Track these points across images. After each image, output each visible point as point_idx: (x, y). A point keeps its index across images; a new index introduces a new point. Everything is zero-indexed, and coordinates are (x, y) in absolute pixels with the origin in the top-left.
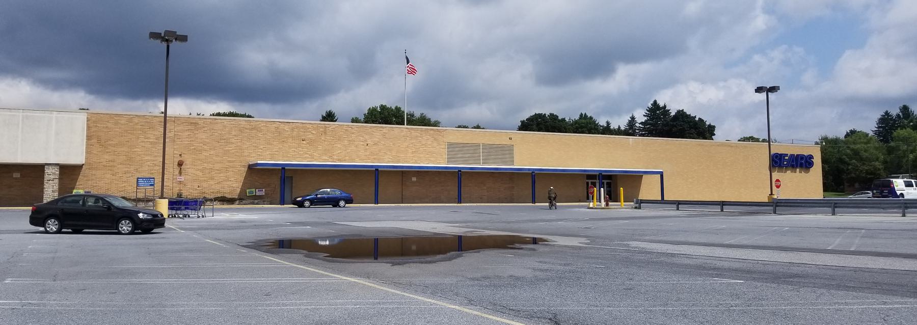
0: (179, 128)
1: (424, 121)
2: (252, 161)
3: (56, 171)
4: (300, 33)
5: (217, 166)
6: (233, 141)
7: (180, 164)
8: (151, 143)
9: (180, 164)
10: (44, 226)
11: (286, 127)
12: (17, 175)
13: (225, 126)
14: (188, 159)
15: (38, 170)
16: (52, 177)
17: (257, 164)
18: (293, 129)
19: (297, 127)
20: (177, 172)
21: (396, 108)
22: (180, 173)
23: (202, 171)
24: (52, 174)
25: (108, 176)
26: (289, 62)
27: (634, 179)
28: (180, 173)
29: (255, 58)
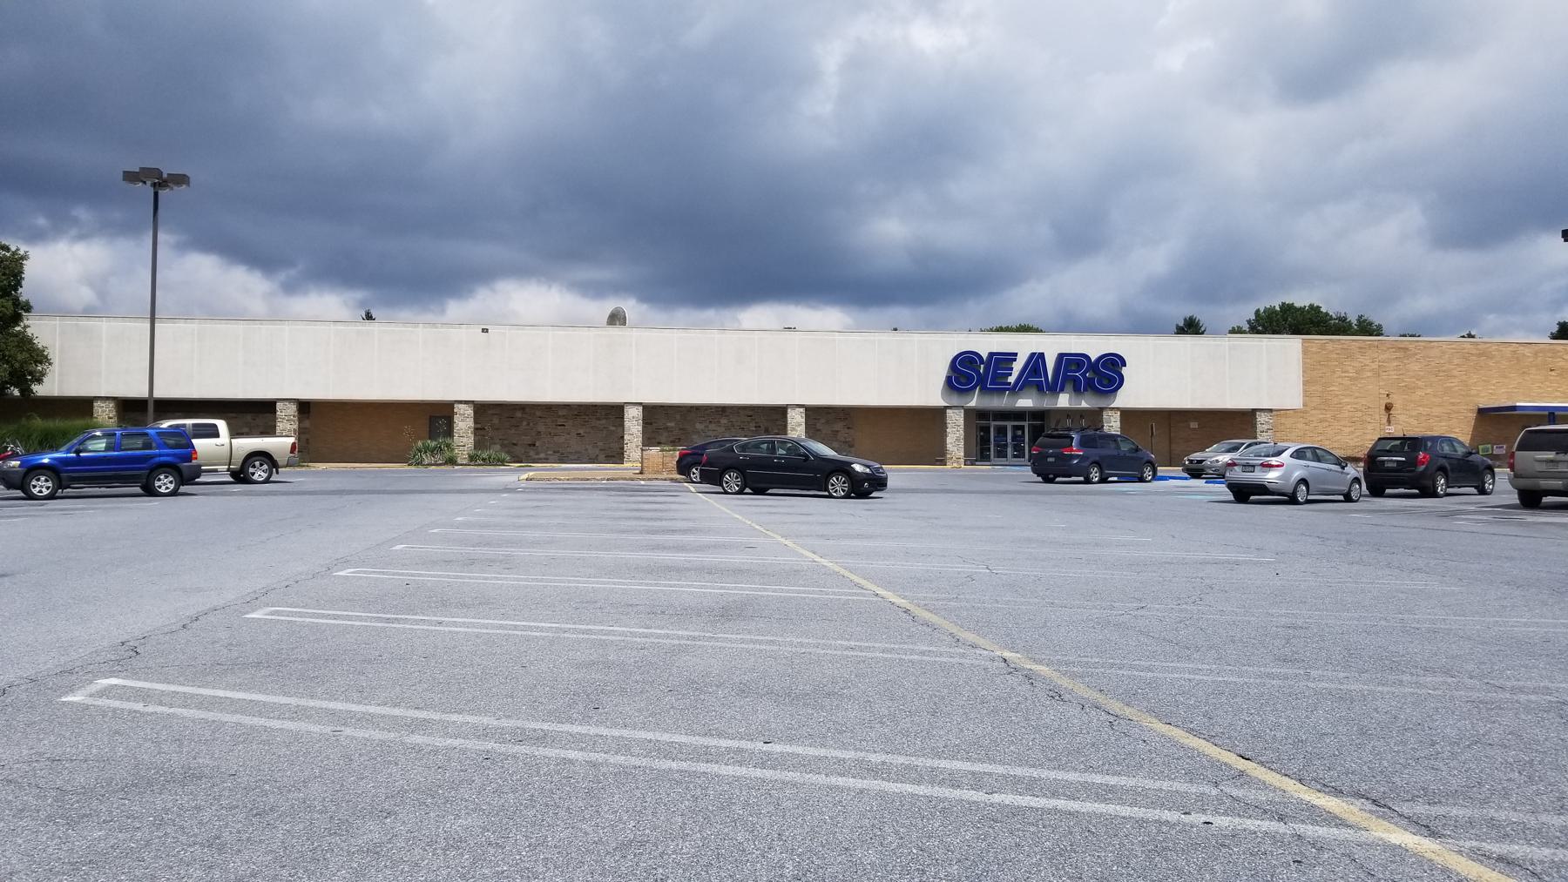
0: (1386, 356)
1: (1366, 328)
2: (1486, 403)
3: (293, 408)
4: (966, 186)
5: (1437, 411)
6: (1455, 373)
7: (1388, 408)
8: (1351, 379)
9: (1388, 408)
10: (826, 490)
11: (1527, 351)
12: (1194, 425)
13: (1444, 353)
14: (1397, 400)
15: (780, 412)
16: (1266, 427)
17: (1514, 408)
18: (1536, 354)
19: (1541, 351)
20: (1385, 420)
21: (1311, 306)
22: (1389, 422)
23: (1417, 417)
24: (105, 414)
25: (1300, 426)
26: (957, 236)
27: (1235, 424)
28: (1389, 422)
29: (890, 231)
